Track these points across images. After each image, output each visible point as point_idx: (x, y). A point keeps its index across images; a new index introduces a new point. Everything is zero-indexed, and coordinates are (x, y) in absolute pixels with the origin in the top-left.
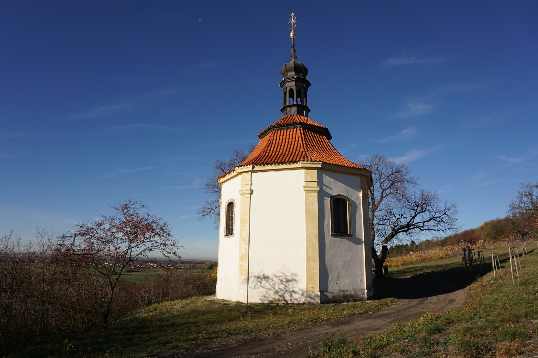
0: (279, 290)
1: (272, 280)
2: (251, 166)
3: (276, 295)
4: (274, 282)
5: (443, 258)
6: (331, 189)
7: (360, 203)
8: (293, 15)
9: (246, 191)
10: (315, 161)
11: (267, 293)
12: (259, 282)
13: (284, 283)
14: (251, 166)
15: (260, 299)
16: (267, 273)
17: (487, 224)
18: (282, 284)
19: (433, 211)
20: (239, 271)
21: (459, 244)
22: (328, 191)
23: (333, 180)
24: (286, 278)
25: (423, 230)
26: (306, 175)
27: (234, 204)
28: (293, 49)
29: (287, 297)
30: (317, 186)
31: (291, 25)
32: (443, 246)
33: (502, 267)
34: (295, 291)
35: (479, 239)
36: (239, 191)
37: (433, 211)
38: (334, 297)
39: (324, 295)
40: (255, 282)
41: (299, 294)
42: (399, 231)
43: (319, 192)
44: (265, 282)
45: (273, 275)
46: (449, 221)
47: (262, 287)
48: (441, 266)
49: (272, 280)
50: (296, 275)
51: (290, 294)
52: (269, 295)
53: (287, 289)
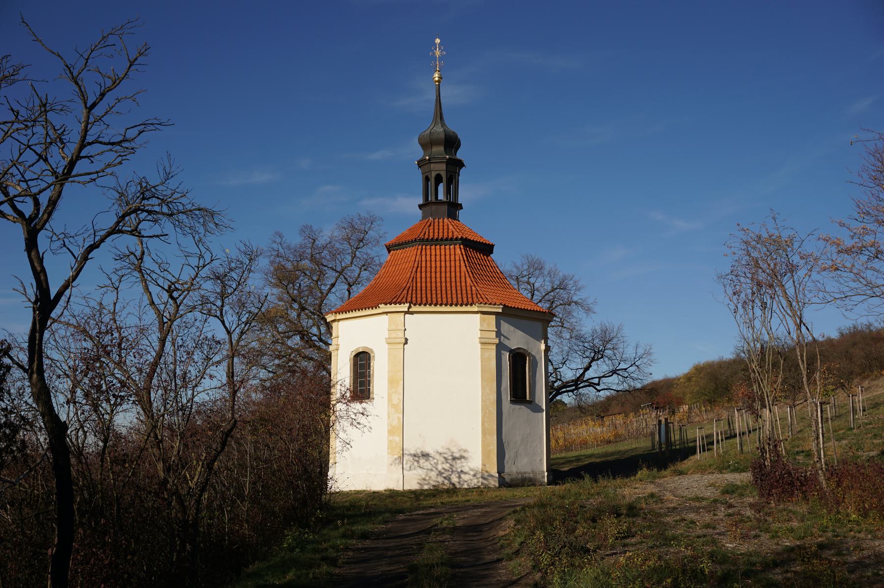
0: (443, 471)
1: (434, 459)
2: (408, 305)
3: (439, 477)
4: (435, 461)
5: (609, 442)
6: (509, 339)
7: (541, 358)
8: (438, 41)
10: (495, 304)
11: (427, 475)
12: (416, 461)
13: (450, 461)
14: (408, 305)
15: (418, 483)
16: (428, 450)
17: (699, 370)
18: (447, 463)
19: (615, 358)
20: (388, 449)
21: (638, 411)
22: (506, 342)
23: (512, 328)
24: (452, 456)
25: (599, 391)
26: (482, 321)
29: (455, 479)
30: (495, 337)
32: (603, 417)
33: (708, 450)
34: (464, 471)
35: (680, 402)
36: (386, 339)
37: (615, 358)
38: (512, 480)
39: (502, 477)
40: (411, 462)
41: (469, 474)
42: (563, 390)
43: (497, 345)
44: (424, 460)
45: (434, 452)
46: (640, 377)
47: (420, 467)
48: (612, 454)
49: (434, 459)
50: (465, 451)
51: (457, 475)
52: (430, 477)
53: (454, 469)
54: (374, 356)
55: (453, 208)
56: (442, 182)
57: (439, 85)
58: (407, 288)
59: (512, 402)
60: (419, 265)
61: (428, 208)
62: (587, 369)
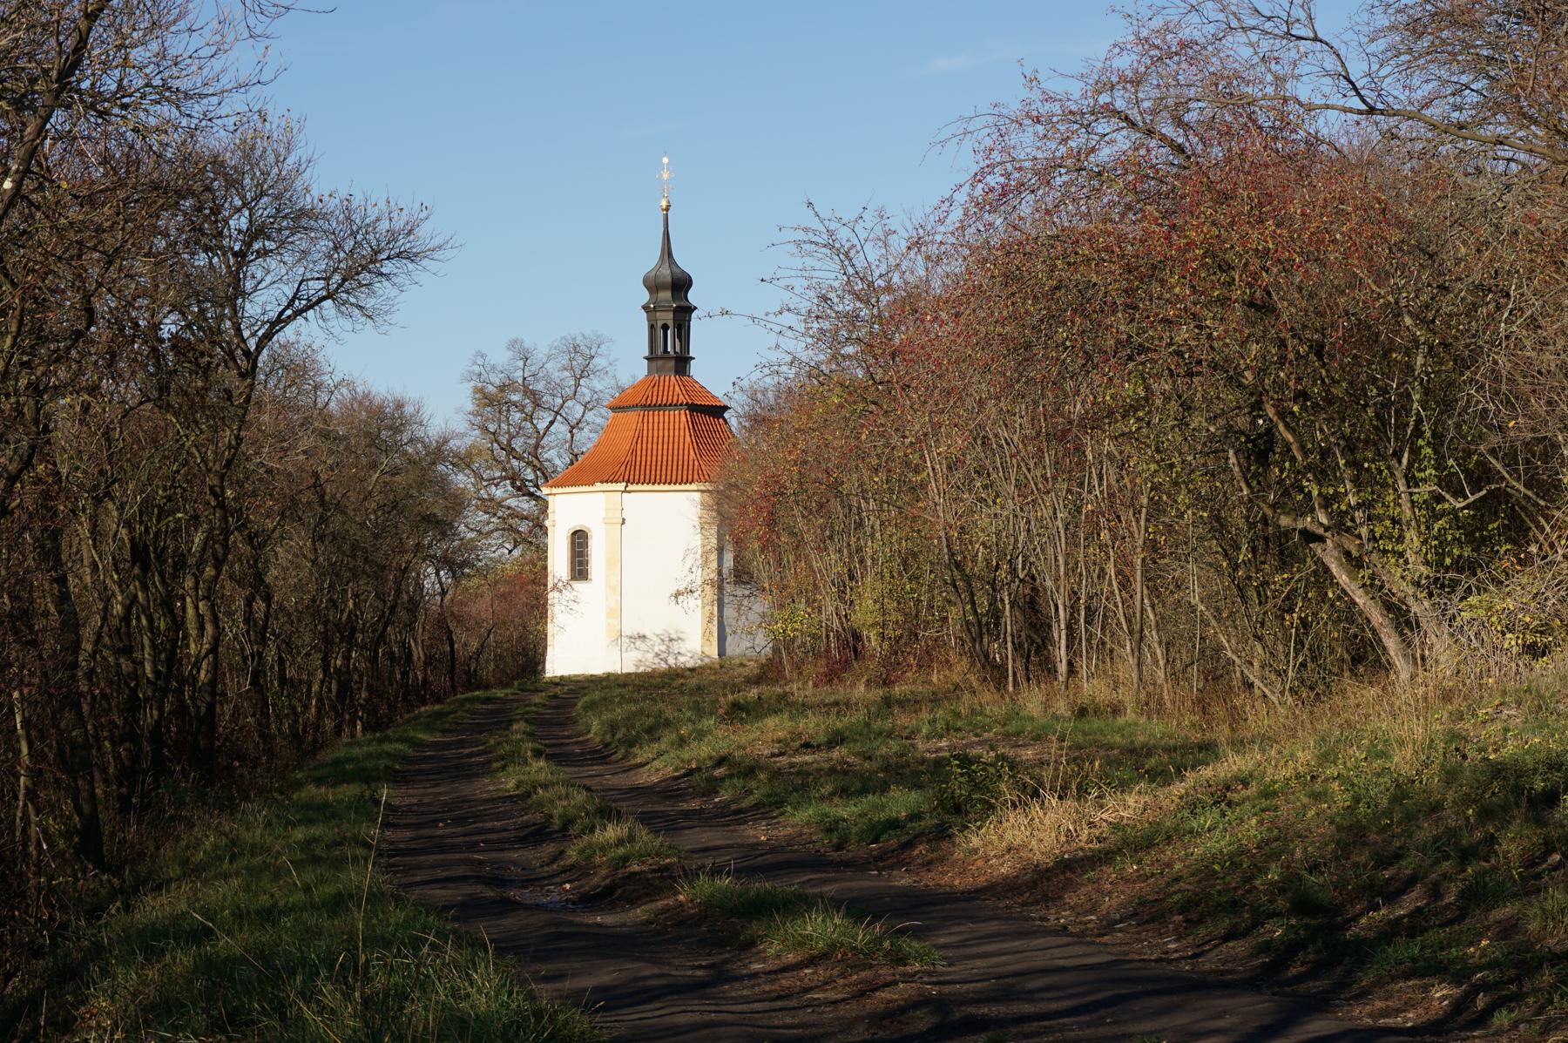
55: (682, 362)
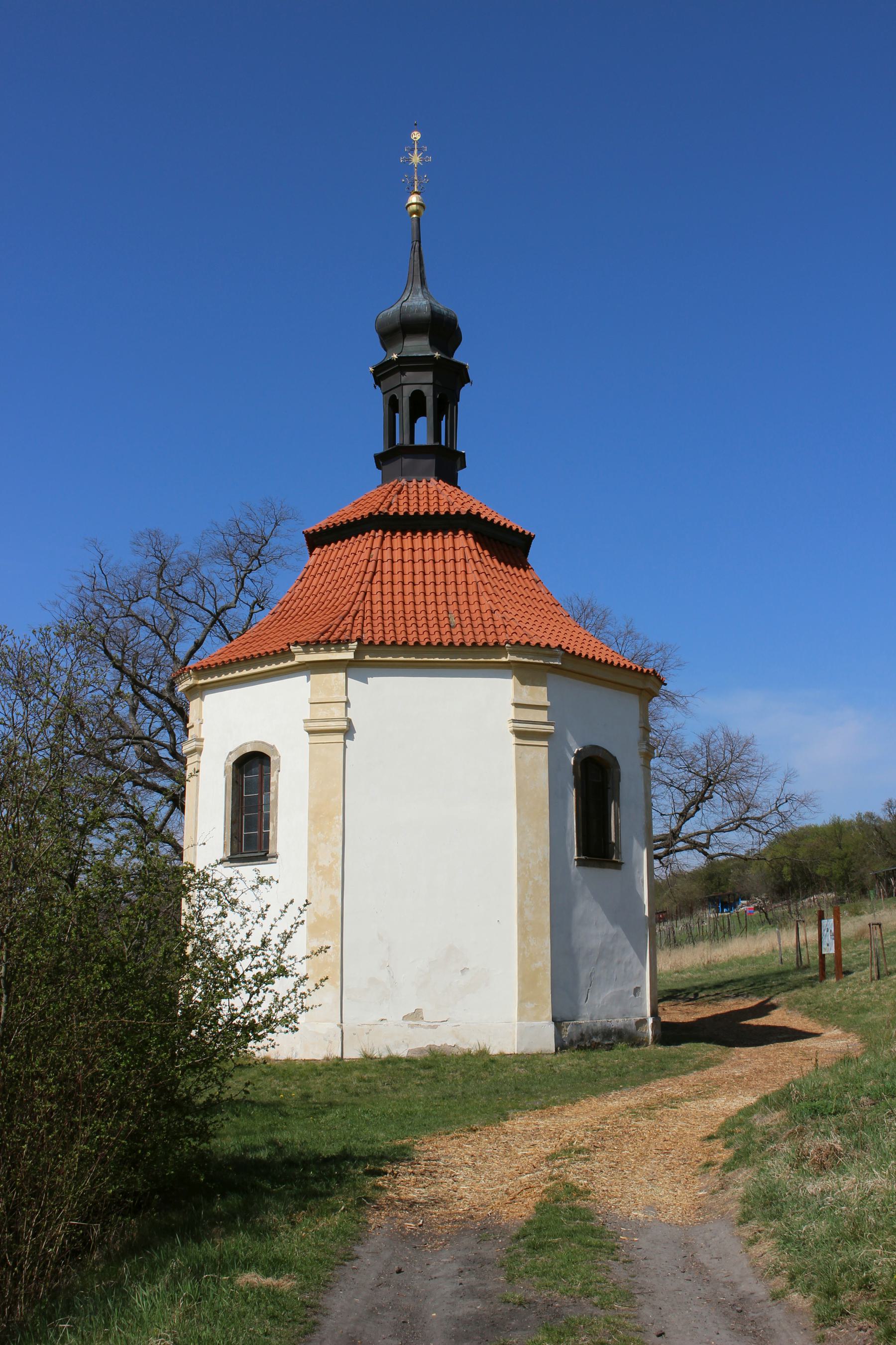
8: (416, 136)
9: (329, 723)
27: (273, 758)
28: (417, 254)
31: (408, 167)
36: (305, 721)
54: (278, 762)
56: (425, 415)
57: (418, 219)
58: (352, 613)
59: (580, 863)
60: (378, 569)
61: (395, 465)
62: (684, 816)
